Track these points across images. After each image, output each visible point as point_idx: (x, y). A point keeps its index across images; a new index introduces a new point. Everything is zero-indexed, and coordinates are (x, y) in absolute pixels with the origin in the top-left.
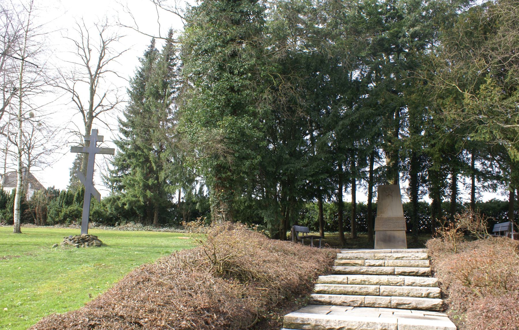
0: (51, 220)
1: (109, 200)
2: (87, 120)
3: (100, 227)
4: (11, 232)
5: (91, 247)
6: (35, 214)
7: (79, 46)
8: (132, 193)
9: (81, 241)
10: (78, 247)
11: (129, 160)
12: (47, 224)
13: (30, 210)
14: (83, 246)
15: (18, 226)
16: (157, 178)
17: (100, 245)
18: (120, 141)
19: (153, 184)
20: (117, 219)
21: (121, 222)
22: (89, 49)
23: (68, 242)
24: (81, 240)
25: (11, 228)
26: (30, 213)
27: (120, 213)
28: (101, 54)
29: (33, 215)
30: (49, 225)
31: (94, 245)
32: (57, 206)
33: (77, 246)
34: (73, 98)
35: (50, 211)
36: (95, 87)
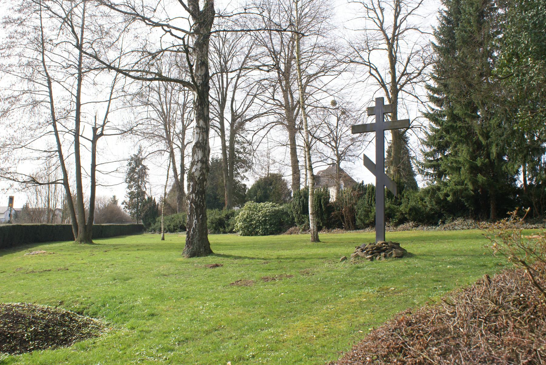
0: (361, 223)
1: (427, 192)
2: (391, 96)
3: (420, 227)
4: (308, 240)
5: (389, 259)
6: (342, 217)
7: (367, 8)
8: (456, 179)
9: (375, 251)
10: (372, 259)
11: (448, 136)
12: (356, 228)
13: (336, 212)
14: (378, 258)
15: (315, 234)
16: (488, 156)
17: (403, 254)
18: (432, 112)
19: (483, 164)
20: (440, 216)
21: (446, 219)
22: (380, 8)
23: (360, 253)
24: (375, 249)
25: (308, 236)
26: (337, 216)
27: (443, 207)
28: (396, 10)
29: (341, 218)
30: (359, 229)
31: (394, 256)
32: (365, 205)
33: (370, 258)
34: (370, 72)
35: (358, 212)
36: (396, 53)
